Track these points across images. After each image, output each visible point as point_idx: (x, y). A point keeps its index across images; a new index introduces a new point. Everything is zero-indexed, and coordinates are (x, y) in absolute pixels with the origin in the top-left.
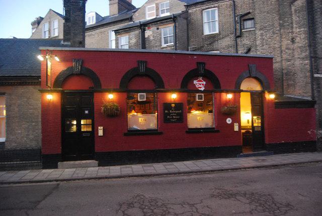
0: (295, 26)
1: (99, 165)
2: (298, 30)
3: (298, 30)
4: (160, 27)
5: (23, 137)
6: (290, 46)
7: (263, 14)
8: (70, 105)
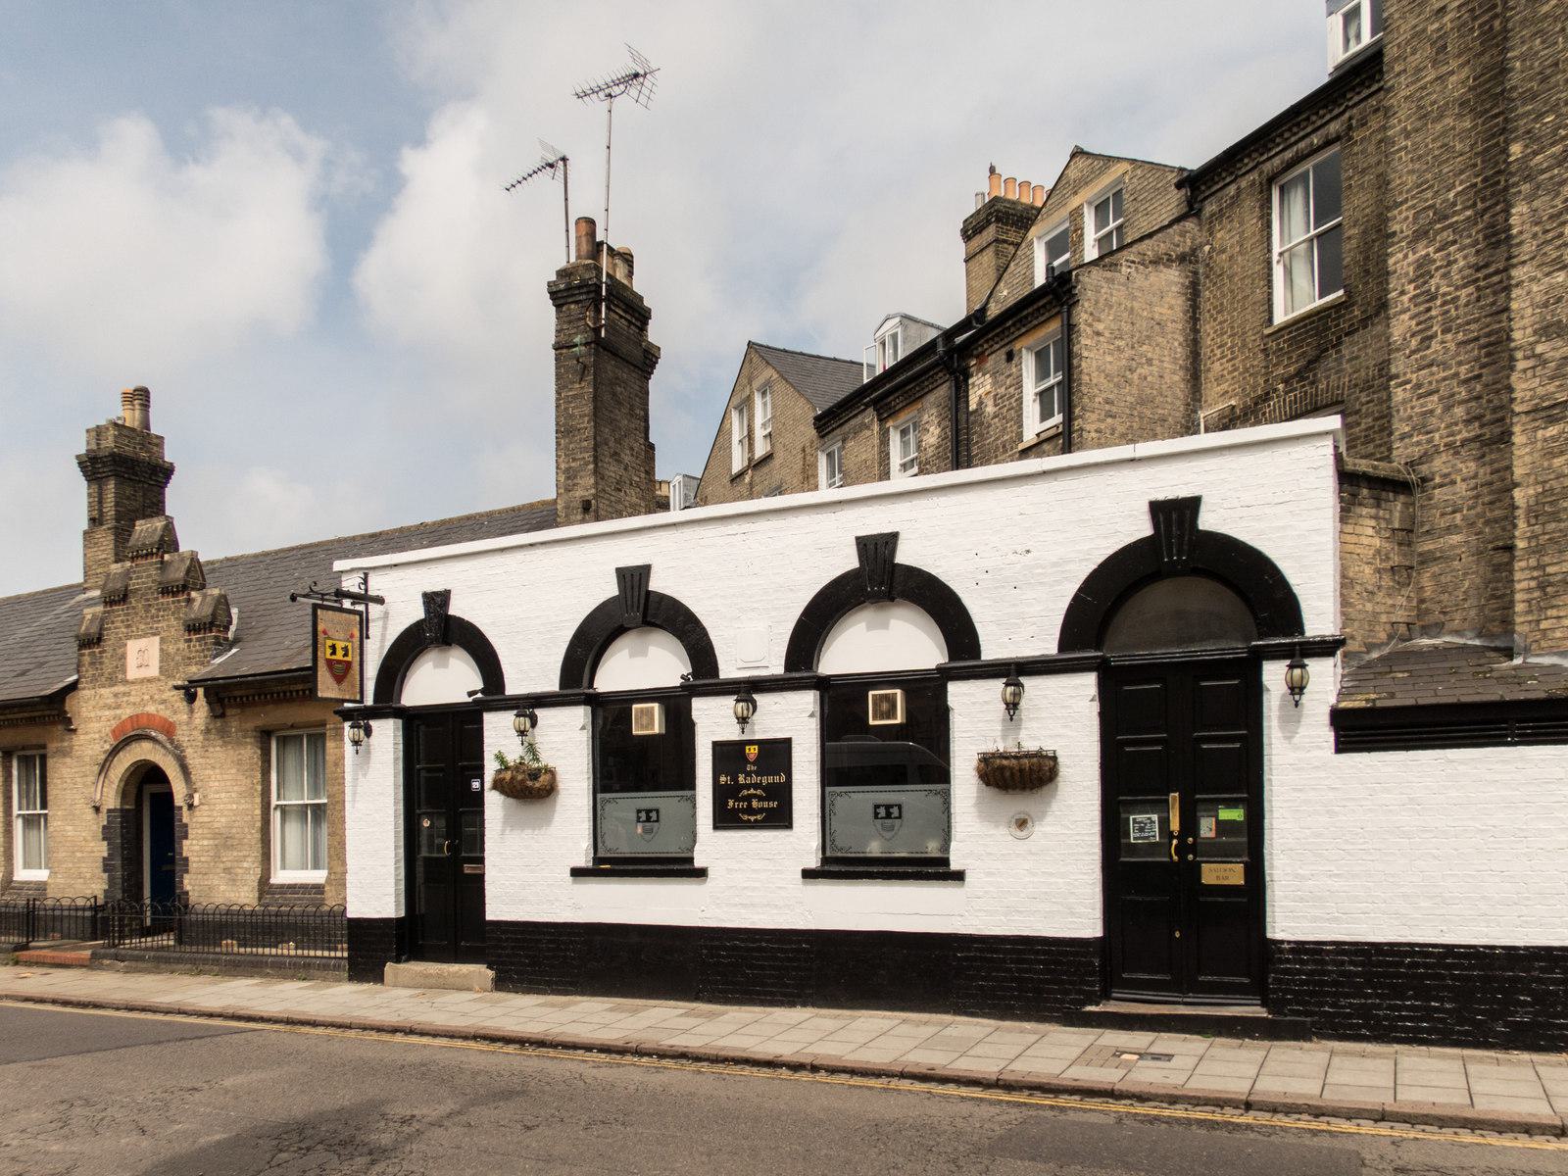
1: (501, 984)
4: (1017, 346)
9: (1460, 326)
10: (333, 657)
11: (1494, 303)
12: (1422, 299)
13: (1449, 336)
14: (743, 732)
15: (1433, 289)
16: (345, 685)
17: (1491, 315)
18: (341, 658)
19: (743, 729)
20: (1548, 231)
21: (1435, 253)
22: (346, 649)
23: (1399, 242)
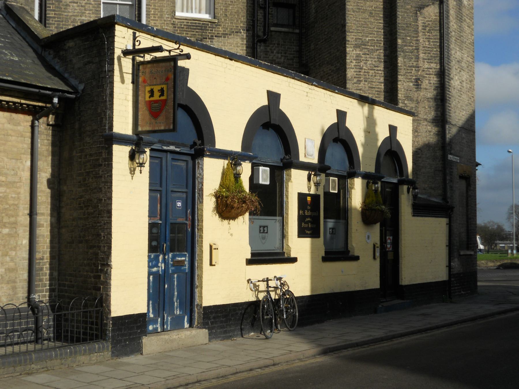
0: (421, 55)
2: (426, 66)
3: (426, 66)
6: (411, 94)
9: (369, 81)
10: (152, 99)
11: (379, 79)
12: (358, 67)
13: (366, 83)
14: (317, 190)
15: (361, 66)
16: (161, 118)
17: (379, 82)
18: (158, 98)
19: (317, 189)
20: (408, 70)
21: (362, 54)
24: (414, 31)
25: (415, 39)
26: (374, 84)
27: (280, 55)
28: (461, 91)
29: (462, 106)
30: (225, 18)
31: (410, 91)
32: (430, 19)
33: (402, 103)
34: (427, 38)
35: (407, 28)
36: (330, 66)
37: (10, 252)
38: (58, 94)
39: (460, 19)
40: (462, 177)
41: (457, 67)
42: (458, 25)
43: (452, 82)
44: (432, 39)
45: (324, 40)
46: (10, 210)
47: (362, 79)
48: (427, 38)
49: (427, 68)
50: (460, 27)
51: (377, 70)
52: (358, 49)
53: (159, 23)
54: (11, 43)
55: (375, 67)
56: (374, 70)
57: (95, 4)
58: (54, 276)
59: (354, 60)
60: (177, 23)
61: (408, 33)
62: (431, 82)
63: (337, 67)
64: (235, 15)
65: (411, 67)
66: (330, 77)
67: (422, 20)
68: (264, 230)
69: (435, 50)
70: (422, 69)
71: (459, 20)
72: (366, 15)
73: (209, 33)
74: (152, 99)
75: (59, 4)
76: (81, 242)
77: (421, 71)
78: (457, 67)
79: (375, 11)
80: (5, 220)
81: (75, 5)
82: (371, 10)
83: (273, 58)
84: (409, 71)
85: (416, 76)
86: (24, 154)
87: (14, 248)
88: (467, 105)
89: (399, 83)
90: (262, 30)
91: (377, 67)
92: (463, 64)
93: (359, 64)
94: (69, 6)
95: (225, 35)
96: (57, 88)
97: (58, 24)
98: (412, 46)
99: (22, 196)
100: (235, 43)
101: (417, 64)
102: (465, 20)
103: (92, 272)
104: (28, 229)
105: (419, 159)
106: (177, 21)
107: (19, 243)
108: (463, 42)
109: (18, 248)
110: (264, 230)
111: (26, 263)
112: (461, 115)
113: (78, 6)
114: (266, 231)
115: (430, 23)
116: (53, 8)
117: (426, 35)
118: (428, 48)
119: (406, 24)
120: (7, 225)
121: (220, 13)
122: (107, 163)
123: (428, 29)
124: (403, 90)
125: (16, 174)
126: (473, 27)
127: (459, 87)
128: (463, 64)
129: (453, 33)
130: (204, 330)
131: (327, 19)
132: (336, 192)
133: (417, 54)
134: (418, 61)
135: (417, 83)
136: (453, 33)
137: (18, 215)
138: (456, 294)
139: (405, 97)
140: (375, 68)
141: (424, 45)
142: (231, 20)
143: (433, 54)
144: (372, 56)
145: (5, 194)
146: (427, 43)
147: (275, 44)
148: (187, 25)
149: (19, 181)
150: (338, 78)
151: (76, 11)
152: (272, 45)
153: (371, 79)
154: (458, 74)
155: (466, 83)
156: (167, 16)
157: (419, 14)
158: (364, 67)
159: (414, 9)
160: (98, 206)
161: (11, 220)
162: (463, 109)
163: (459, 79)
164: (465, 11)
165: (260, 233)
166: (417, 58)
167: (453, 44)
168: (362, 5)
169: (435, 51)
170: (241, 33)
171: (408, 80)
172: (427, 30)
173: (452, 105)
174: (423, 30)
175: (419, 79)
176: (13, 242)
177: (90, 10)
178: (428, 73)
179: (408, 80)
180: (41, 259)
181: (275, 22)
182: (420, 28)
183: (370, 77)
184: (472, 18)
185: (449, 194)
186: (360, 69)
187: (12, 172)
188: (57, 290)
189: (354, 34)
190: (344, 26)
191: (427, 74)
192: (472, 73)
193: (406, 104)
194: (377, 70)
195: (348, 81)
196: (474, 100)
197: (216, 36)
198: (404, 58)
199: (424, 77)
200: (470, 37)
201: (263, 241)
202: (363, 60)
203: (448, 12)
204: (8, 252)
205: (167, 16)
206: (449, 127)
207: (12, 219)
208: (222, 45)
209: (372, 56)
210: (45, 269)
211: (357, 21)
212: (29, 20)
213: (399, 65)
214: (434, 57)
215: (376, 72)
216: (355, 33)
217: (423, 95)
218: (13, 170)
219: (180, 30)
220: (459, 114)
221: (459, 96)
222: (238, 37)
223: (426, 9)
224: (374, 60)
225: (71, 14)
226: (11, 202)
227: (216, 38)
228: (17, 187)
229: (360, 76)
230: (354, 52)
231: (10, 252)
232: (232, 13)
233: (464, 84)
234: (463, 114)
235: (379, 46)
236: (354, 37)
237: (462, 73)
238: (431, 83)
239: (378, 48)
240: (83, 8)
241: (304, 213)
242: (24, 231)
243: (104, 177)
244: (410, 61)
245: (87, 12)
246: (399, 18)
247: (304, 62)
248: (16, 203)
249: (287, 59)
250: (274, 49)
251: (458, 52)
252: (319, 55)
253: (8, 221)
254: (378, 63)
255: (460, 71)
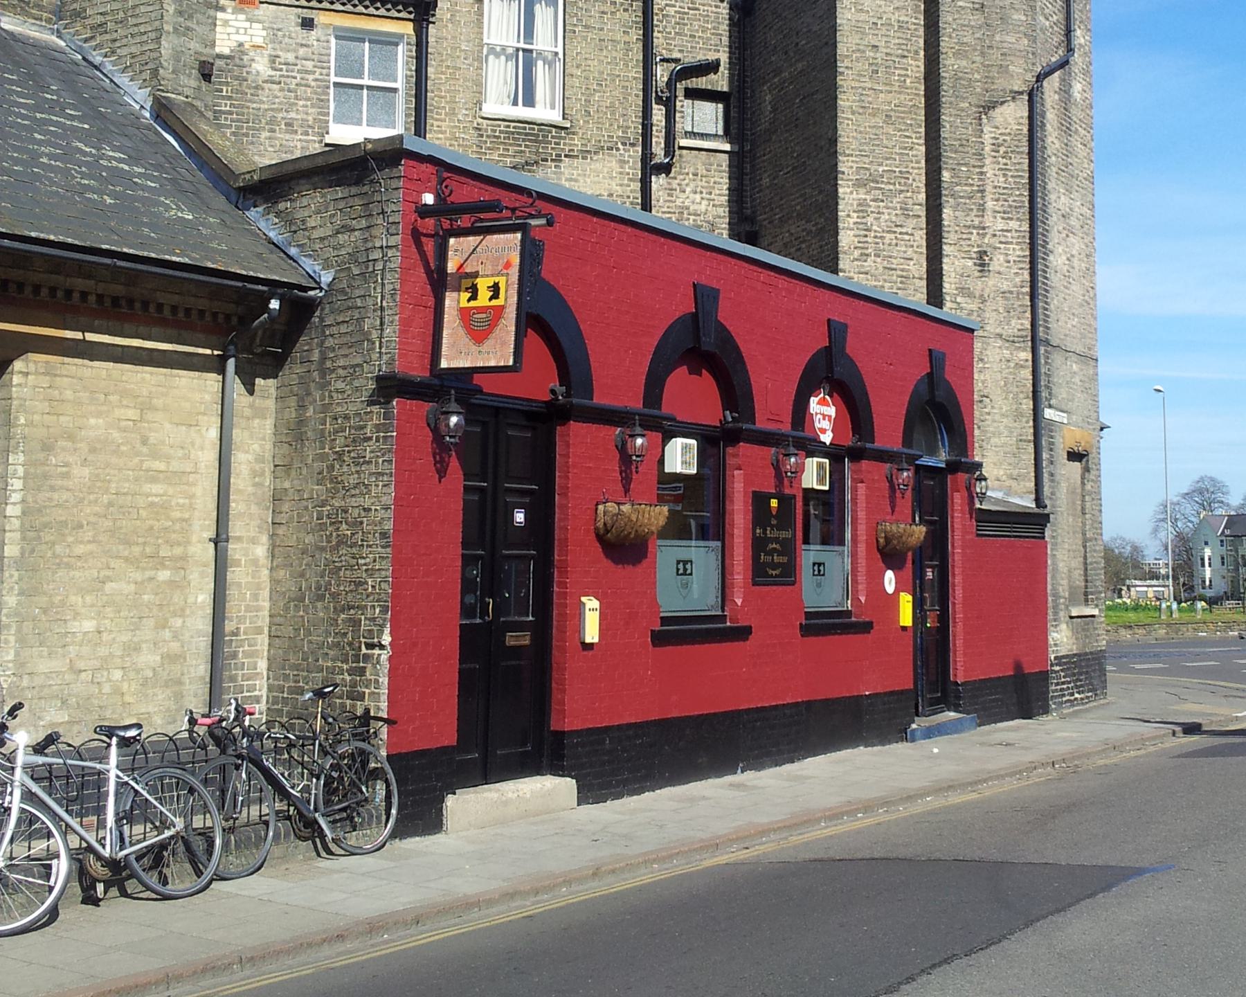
0: (990, 204)
2: (1000, 224)
3: (1000, 224)
4: (321, 18)
5: (105, 664)
6: (970, 283)
7: (873, 121)
8: (936, 434)
10: (473, 304)
11: (905, 252)
12: (861, 226)
13: (879, 260)
22: (495, 289)
23: (848, 180)
24: (974, 154)
25: (978, 170)
26: (894, 261)
27: (698, 197)
28: (1069, 277)
29: (1070, 308)
30: (586, 119)
31: (968, 276)
32: (1008, 131)
33: (952, 301)
34: (1002, 169)
35: (961, 149)
36: (803, 222)
37: (172, 620)
38: (280, 291)
39: (1066, 129)
40: (1074, 456)
41: (1061, 228)
42: (1062, 142)
43: (1051, 258)
44: (1010, 170)
45: (790, 168)
46: (174, 532)
47: (870, 251)
48: (1002, 169)
49: (1002, 230)
50: (1066, 145)
51: (901, 233)
52: (862, 190)
53: (448, 126)
54: (173, 181)
55: (897, 226)
56: (895, 232)
57: (319, 87)
58: (258, 670)
59: (854, 211)
60: (485, 126)
61: (963, 159)
62: (1011, 258)
63: (819, 226)
64: (606, 113)
65: (969, 227)
66: (803, 246)
67: (991, 132)
68: (685, 570)
69: (1018, 193)
70: (990, 231)
71: (1065, 132)
72: (879, 121)
73: (552, 148)
74: (473, 304)
75: (240, 85)
76: (321, 598)
77: (988, 236)
78: (1061, 228)
79: (898, 112)
80: (162, 554)
81: (275, 86)
82: (888, 111)
83: (683, 202)
84: (964, 236)
85: (978, 246)
86: (205, 414)
87: (181, 613)
88: (1081, 306)
89: (945, 260)
90: (663, 145)
91: (901, 226)
92: (1073, 221)
93: (864, 220)
94: (263, 89)
95: (585, 154)
96: (277, 278)
97: (237, 127)
98: (972, 185)
99: (199, 503)
100: (606, 170)
101: (981, 223)
102: (1076, 132)
103: (346, 661)
104: (211, 570)
105: (987, 417)
106: (485, 122)
107: (191, 600)
108: (1072, 176)
109: (188, 612)
110: (685, 570)
111: (204, 643)
112: (1069, 326)
113: (282, 90)
114: (689, 572)
115: (1008, 138)
116: (227, 92)
117: (999, 163)
118: (1004, 188)
119: (960, 140)
120: (167, 563)
121: (575, 108)
122: (382, 434)
123: (1002, 149)
124: (953, 275)
125: (187, 457)
126: (1093, 144)
127: (1066, 268)
128: (1073, 221)
129: (1054, 158)
130: (569, 779)
131: (796, 126)
132: (826, 488)
133: (981, 202)
134: (983, 216)
135: (982, 261)
136: (1054, 158)
137: (188, 542)
138: (1064, 699)
139: (957, 289)
140: (895, 229)
141: (996, 184)
142: (599, 123)
143: (1014, 201)
144: (890, 205)
145: (164, 498)
146: (1002, 179)
147: (688, 174)
148: (507, 132)
149: (193, 470)
150: (821, 247)
151: (277, 100)
152: (682, 177)
153: (889, 251)
154: (1063, 243)
155: (1080, 260)
156: (464, 112)
157: (985, 121)
158: (875, 228)
159: (974, 109)
160: (362, 523)
161: (174, 552)
162: (1073, 314)
163: (1066, 252)
164: (1076, 113)
165: (678, 574)
166: (982, 209)
167: (1053, 181)
168: (870, 99)
169: (1017, 196)
170: (618, 149)
171: (963, 255)
172: (1001, 152)
173: (1052, 306)
174: (993, 154)
175: (985, 252)
176: (177, 598)
177: (307, 99)
178: (1003, 239)
179: (963, 255)
180: (235, 634)
181: (690, 129)
182: (988, 148)
183: (886, 247)
184: (1089, 127)
185: (1047, 490)
186: (865, 230)
187: (180, 453)
188: (265, 698)
189: (854, 159)
190: (834, 141)
191: (1001, 242)
192: (1090, 238)
193: (959, 304)
194: (901, 233)
195: (841, 256)
196: (1095, 295)
197: (566, 156)
198: (955, 208)
199: (995, 248)
200: (1086, 166)
201: (819, 590)
202: (872, 212)
203: (1043, 115)
204: (166, 620)
205: (464, 112)
206: (1046, 351)
207: (178, 551)
208: (579, 175)
209: (890, 205)
210: (240, 655)
211: (861, 132)
212: (208, 131)
213: (945, 223)
214: (1016, 207)
215: (899, 236)
216: (856, 156)
217: (994, 286)
218: (182, 448)
219: (491, 142)
220: (1066, 323)
221: (1066, 288)
222: (611, 159)
223: (999, 110)
224: (894, 213)
225: (266, 107)
226: (177, 515)
227: (567, 159)
228: (187, 484)
229: (866, 245)
230: (855, 195)
231: (172, 620)
232: (600, 109)
233: (1076, 262)
234: (1074, 323)
235: (905, 183)
236: (855, 165)
237: (1072, 239)
238: (1009, 262)
239: (902, 188)
240: (293, 94)
241: (765, 533)
242: (202, 575)
243: (377, 463)
244: (968, 215)
245: (301, 103)
246: (944, 127)
247: (749, 212)
248: (186, 516)
249: (713, 206)
250: (687, 185)
251: (1063, 197)
252: (781, 199)
253: (170, 554)
254: (902, 218)
255: (1067, 236)
